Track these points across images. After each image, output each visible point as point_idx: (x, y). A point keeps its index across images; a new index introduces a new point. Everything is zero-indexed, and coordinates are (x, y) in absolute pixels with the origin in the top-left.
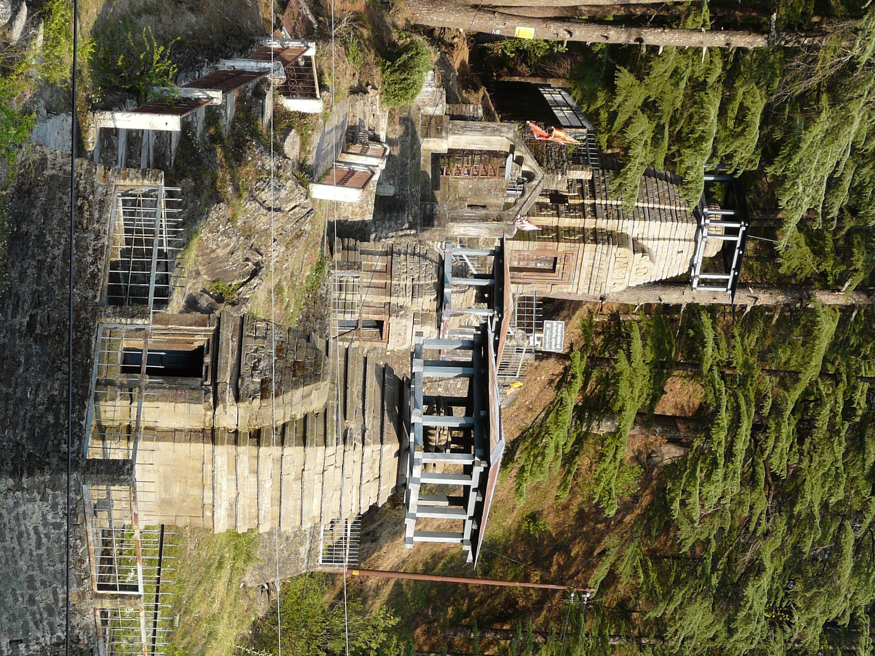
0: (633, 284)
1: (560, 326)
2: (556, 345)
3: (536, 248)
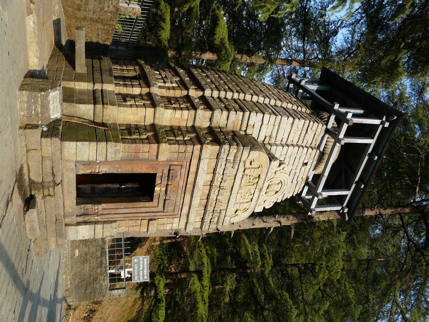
0: (259, 209)
1: (146, 260)
2: (143, 276)
3: (119, 156)
